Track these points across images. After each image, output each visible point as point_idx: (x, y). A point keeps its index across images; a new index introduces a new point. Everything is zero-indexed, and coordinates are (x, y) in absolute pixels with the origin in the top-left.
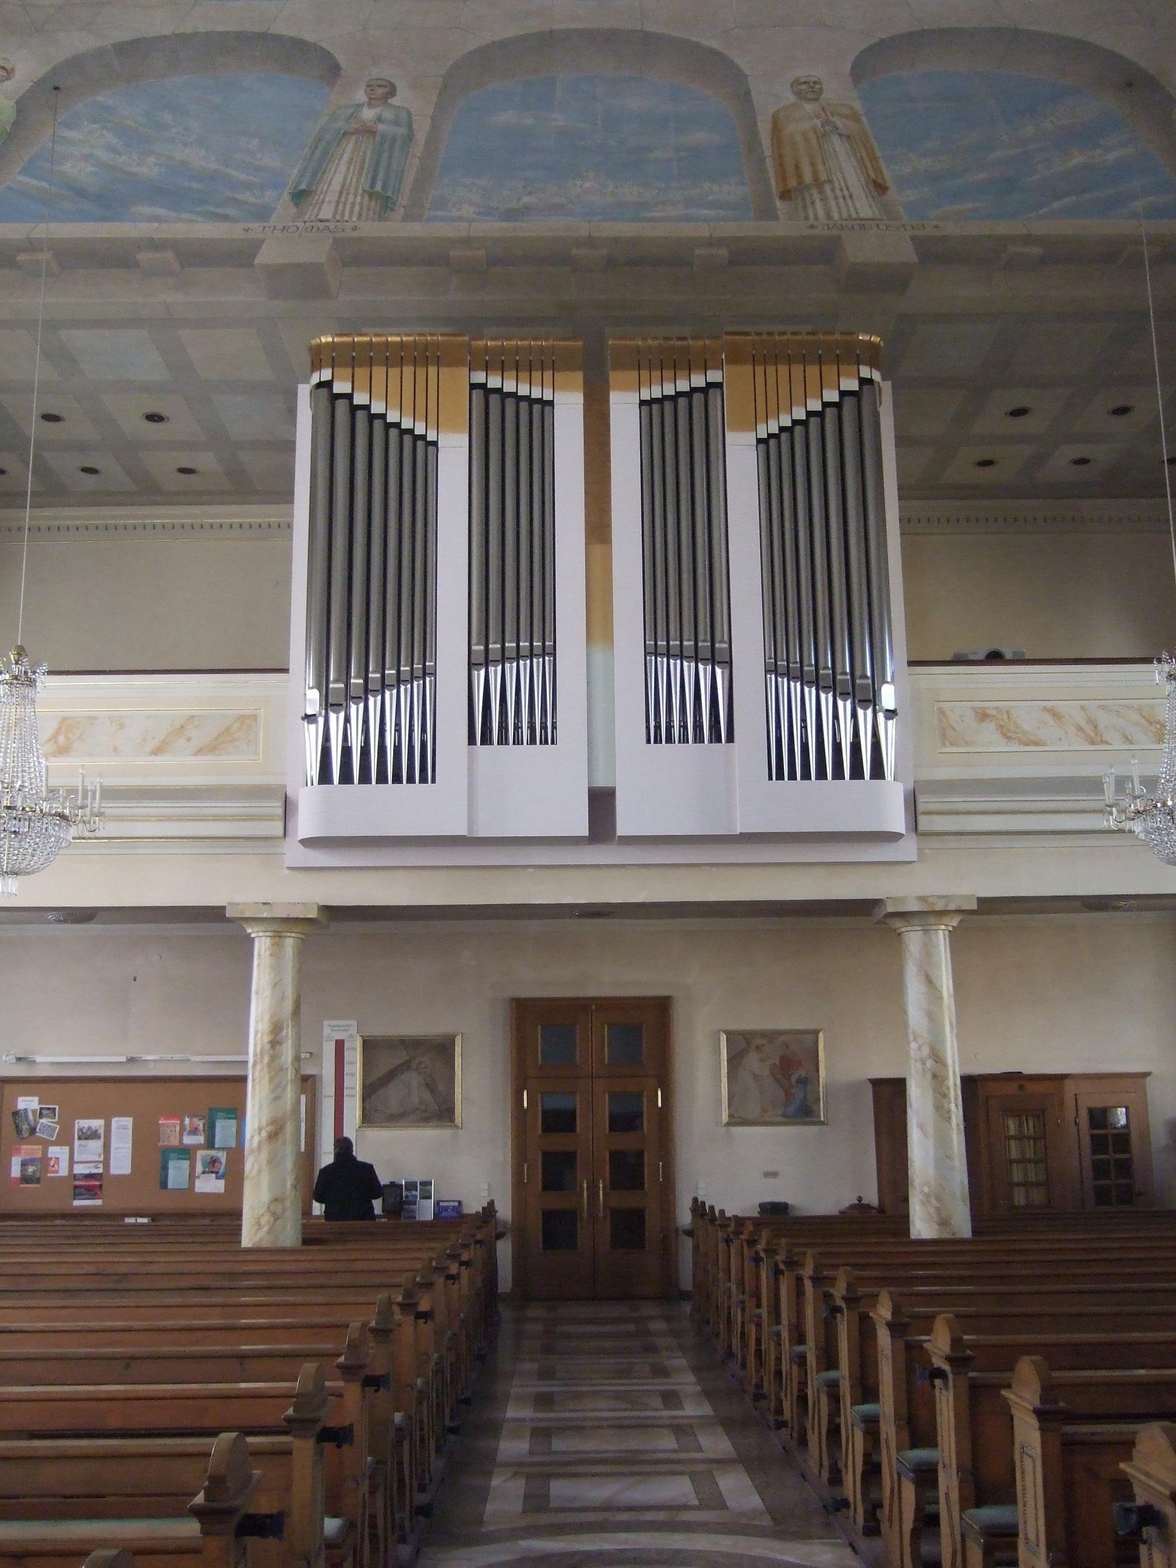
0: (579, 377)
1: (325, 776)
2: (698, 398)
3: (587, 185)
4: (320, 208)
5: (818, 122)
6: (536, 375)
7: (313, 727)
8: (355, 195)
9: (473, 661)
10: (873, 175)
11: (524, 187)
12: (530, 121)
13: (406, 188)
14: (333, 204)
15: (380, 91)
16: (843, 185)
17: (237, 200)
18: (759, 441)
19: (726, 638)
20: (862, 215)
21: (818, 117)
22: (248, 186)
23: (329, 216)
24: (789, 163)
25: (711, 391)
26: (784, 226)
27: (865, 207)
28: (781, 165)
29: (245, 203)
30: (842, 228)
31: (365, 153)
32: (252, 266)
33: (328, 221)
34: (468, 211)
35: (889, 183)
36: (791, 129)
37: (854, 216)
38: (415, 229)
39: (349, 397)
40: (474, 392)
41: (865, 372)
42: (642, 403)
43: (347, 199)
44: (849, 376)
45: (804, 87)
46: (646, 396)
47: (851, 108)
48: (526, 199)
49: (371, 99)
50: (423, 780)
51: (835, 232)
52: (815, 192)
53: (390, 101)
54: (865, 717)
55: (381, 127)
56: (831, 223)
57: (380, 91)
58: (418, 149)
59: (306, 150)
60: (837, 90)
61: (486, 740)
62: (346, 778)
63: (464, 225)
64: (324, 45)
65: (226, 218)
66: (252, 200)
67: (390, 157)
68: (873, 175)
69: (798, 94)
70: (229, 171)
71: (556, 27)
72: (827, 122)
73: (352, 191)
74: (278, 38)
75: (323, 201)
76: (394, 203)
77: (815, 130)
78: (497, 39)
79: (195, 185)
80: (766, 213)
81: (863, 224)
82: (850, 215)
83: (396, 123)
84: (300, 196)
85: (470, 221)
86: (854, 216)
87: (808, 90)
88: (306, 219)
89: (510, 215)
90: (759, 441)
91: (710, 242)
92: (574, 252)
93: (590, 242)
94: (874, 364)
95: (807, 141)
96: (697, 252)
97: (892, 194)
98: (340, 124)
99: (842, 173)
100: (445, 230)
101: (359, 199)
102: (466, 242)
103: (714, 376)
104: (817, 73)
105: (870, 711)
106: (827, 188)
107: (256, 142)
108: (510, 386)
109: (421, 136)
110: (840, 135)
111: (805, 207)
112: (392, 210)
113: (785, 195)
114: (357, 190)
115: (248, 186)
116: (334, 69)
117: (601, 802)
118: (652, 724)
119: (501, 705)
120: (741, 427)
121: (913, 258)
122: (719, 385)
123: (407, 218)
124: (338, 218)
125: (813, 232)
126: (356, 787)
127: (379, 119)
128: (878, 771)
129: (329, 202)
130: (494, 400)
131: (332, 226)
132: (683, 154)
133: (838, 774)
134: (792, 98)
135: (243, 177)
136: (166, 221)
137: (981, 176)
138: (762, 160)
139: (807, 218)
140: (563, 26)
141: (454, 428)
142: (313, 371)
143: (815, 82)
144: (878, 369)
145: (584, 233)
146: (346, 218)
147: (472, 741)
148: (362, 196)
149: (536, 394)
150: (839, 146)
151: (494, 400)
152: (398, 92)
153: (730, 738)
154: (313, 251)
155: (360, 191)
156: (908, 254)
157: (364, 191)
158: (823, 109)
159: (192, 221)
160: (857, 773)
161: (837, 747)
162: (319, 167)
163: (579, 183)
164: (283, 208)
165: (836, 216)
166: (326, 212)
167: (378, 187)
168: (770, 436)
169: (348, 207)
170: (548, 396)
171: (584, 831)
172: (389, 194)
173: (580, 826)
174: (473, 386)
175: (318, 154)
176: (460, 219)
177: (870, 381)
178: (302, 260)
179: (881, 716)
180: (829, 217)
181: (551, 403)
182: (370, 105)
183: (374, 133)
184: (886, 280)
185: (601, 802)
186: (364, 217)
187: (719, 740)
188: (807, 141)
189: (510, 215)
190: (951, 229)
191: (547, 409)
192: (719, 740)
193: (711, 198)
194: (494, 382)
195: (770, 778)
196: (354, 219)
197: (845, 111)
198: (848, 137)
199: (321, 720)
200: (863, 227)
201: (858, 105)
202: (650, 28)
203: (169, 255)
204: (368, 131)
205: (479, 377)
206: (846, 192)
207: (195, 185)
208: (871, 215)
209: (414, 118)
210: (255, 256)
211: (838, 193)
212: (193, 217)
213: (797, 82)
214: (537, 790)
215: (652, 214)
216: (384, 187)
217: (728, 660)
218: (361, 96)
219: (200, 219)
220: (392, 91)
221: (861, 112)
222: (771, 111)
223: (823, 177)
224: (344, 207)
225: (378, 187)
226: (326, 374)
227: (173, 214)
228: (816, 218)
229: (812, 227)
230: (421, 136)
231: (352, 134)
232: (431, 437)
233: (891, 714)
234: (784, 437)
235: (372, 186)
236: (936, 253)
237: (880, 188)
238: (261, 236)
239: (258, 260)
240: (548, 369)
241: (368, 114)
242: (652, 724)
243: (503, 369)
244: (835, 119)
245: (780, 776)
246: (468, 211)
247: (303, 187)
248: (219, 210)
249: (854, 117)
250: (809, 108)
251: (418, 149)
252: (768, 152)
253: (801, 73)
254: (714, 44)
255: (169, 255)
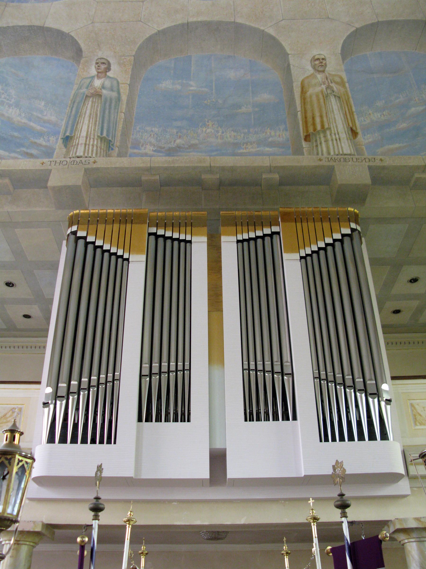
0: (205, 229)
1: (51, 439)
2: (268, 239)
3: (209, 130)
4: (77, 148)
5: (324, 87)
6: (183, 229)
7: (46, 410)
8: (94, 141)
9: (143, 374)
10: (351, 125)
11: (177, 133)
12: (179, 87)
13: (119, 134)
14: (83, 146)
15: (103, 67)
16: (336, 132)
17: (35, 143)
18: (301, 258)
19: (289, 360)
20: (345, 152)
21: (324, 84)
22: (41, 134)
23: (82, 154)
24: (309, 115)
25: (274, 236)
26: (306, 160)
27: (346, 147)
28: (306, 118)
29: (41, 145)
30: (335, 160)
31: (97, 110)
32: (46, 187)
33: (81, 157)
34: (149, 149)
35: (359, 131)
36: (311, 91)
37: (341, 152)
38: (124, 162)
39: (85, 238)
40: (150, 237)
41: (353, 225)
42: (238, 241)
43: (90, 142)
44: (345, 227)
45: (317, 62)
46: (240, 238)
47: (341, 78)
48: (178, 141)
49: (98, 72)
50: (109, 442)
51: (331, 163)
52: (322, 135)
53: (108, 74)
54: (373, 403)
55: (104, 92)
56: (330, 157)
57: (103, 67)
58: (123, 106)
59: (68, 108)
60: (334, 66)
61: (149, 419)
62: (63, 440)
63: (148, 159)
64: (72, 34)
65: (31, 156)
66: (44, 143)
67: (110, 112)
68: (351, 125)
69: (314, 67)
70: (32, 124)
71: (191, 20)
72: (328, 87)
73: (92, 137)
74: (49, 30)
75: (78, 144)
76: (113, 145)
77: (322, 92)
78: (161, 29)
79: (16, 134)
80: (298, 151)
81: (345, 158)
82: (339, 152)
83: (112, 89)
84: (67, 140)
85: (151, 156)
86: (341, 152)
87: (319, 64)
88: (71, 156)
89: (171, 152)
90: (301, 258)
91: (271, 170)
92: (203, 177)
93: (210, 170)
94: (357, 222)
95: (318, 100)
96: (264, 176)
97: (360, 137)
98: (84, 90)
99: (335, 123)
100: (139, 162)
101: (95, 143)
102: (149, 170)
103: (275, 229)
104: (324, 52)
105: (376, 400)
106: (328, 133)
107: (43, 103)
108: (168, 234)
109: (124, 98)
110: (335, 96)
111: (317, 146)
112: (112, 149)
113: (307, 138)
114: (94, 136)
115: (41, 134)
116: (78, 53)
117: (218, 459)
118: (248, 411)
119: (158, 400)
120: (291, 250)
121: (368, 181)
122: (278, 233)
123: (120, 155)
124: (86, 155)
125: (321, 163)
126: (68, 446)
127: (103, 87)
128: (384, 436)
129: (81, 144)
130: (161, 240)
131: (83, 159)
132: (256, 109)
133: (361, 437)
134: (310, 70)
135: (38, 128)
136: (4, 159)
137: (404, 125)
138: (296, 116)
139: (318, 154)
140: (195, 19)
141: (139, 252)
142: (69, 228)
143: (323, 59)
144: (359, 225)
145: (207, 164)
146: (90, 155)
147: (140, 419)
148: (97, 140)
149: (182, 237)
150: (334, 103)
151: (161, 240)
152: (112, 67)
153: (295, 418)
154: (75, 178)
155: (96, 137)
156: (365, 178)
157: (98, 136)
158: (327, 78)
159: (17, 158)
160: (372, 437)
161: (359, 423)
162: (74, 121)
163: (204, 129)
164: (59, 145)
165: (332, 153)
166: (80, 152)
167: (105, 134)
168: (307, 255)
169: (91, 147)
170: (188, 238)
171: (206, 475)
172: (110, 139)
173: (204, 472)
174: (150, 234)
175: (74, 109)
176: (146, 155)
177: (356, 230)
178: (70, 184)
179: (383, 404)
180: (329, 154)
181: (190, 242)
182: (99, 77)
183: (100, 96)
184: (358, 195)
185: (218, 459)
186: (99, 155)
187: (288, 419)
188: (318, 100)
189: (171, 152)
190: (388, 162)
191: (188, 244)
192: (288, 419)
193: (270, 139)
194: (161, 232)
195: (321, 441)
196: (94, 155)
197: (337, 79)
198: (339, 97)
199: (52, 406)
200: (345, 160)
201: (344, 75)
202: (239, 20)
203: (7, 181)
204: (98, 95)
205: (153, 230)
206: (337, 136)
207: (16, 134)
208: (349, 152)
209: (120, 85)
210: (47, 181)
211: (334, 137)
212: (16, 155)
213: (314, 59)
214: (179, 452)
215: (241, 151)
216: (108, 135)
217: (291, 372)
218: (93, 71)
219: (20, 157)
220: (108, 69)
221: (346, 80)
222: (301, 79)
223: (326, 126)
224: (89, 148)
225: (105, 134)
226: (74, 228)
227: (7, 154)
228: (322, 155)
229: (320, 160)
230: (124, 98)
231: (90, 97)
232: (126, 256)
233: (388, 401)
234: (315, 255)
235: (102, 133)
236: (382, 178)
237: (354, 133)
238: (50, 168)
239: (50, 184)
240: (189, 226)
241: (97, 83)
242: (248, 411)
243: (165, 227)
244: (333, 85)
245: (326, 440)
246: (149, 149)
247: (68, 134)
248: (29, 151)
249: (342, 83)
250: (320, 76)
251: (123, 106)
252: (299, 108)
253: (315, 52)
254: (271, 31)
255: (7, 181)
